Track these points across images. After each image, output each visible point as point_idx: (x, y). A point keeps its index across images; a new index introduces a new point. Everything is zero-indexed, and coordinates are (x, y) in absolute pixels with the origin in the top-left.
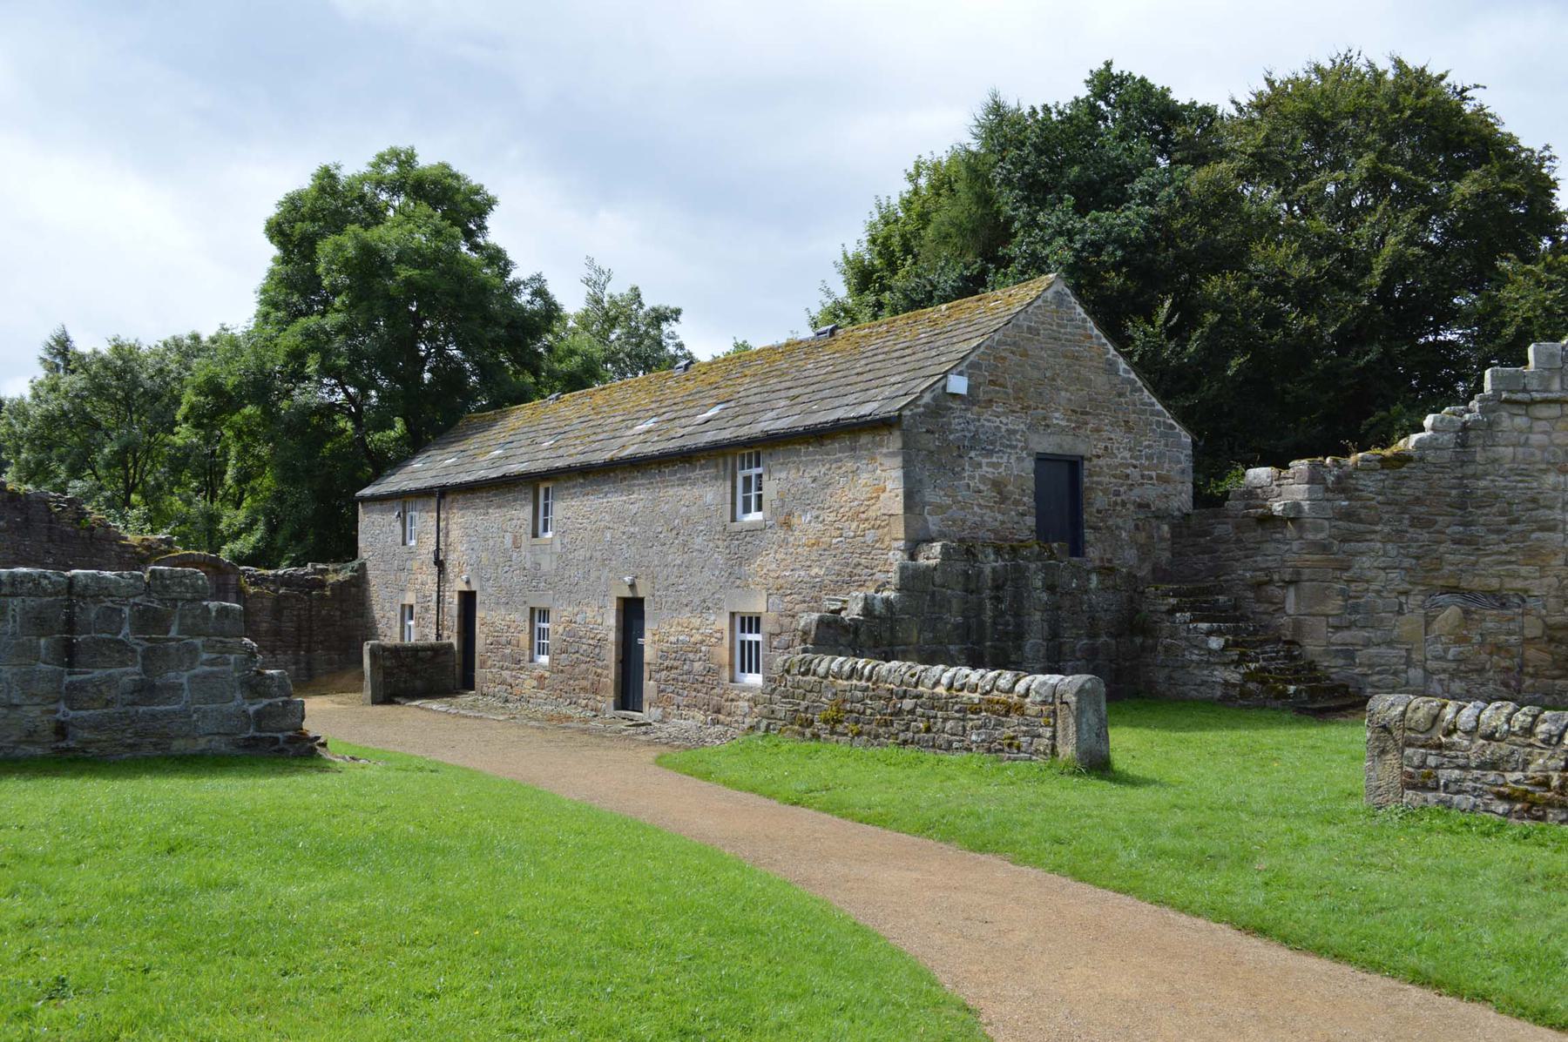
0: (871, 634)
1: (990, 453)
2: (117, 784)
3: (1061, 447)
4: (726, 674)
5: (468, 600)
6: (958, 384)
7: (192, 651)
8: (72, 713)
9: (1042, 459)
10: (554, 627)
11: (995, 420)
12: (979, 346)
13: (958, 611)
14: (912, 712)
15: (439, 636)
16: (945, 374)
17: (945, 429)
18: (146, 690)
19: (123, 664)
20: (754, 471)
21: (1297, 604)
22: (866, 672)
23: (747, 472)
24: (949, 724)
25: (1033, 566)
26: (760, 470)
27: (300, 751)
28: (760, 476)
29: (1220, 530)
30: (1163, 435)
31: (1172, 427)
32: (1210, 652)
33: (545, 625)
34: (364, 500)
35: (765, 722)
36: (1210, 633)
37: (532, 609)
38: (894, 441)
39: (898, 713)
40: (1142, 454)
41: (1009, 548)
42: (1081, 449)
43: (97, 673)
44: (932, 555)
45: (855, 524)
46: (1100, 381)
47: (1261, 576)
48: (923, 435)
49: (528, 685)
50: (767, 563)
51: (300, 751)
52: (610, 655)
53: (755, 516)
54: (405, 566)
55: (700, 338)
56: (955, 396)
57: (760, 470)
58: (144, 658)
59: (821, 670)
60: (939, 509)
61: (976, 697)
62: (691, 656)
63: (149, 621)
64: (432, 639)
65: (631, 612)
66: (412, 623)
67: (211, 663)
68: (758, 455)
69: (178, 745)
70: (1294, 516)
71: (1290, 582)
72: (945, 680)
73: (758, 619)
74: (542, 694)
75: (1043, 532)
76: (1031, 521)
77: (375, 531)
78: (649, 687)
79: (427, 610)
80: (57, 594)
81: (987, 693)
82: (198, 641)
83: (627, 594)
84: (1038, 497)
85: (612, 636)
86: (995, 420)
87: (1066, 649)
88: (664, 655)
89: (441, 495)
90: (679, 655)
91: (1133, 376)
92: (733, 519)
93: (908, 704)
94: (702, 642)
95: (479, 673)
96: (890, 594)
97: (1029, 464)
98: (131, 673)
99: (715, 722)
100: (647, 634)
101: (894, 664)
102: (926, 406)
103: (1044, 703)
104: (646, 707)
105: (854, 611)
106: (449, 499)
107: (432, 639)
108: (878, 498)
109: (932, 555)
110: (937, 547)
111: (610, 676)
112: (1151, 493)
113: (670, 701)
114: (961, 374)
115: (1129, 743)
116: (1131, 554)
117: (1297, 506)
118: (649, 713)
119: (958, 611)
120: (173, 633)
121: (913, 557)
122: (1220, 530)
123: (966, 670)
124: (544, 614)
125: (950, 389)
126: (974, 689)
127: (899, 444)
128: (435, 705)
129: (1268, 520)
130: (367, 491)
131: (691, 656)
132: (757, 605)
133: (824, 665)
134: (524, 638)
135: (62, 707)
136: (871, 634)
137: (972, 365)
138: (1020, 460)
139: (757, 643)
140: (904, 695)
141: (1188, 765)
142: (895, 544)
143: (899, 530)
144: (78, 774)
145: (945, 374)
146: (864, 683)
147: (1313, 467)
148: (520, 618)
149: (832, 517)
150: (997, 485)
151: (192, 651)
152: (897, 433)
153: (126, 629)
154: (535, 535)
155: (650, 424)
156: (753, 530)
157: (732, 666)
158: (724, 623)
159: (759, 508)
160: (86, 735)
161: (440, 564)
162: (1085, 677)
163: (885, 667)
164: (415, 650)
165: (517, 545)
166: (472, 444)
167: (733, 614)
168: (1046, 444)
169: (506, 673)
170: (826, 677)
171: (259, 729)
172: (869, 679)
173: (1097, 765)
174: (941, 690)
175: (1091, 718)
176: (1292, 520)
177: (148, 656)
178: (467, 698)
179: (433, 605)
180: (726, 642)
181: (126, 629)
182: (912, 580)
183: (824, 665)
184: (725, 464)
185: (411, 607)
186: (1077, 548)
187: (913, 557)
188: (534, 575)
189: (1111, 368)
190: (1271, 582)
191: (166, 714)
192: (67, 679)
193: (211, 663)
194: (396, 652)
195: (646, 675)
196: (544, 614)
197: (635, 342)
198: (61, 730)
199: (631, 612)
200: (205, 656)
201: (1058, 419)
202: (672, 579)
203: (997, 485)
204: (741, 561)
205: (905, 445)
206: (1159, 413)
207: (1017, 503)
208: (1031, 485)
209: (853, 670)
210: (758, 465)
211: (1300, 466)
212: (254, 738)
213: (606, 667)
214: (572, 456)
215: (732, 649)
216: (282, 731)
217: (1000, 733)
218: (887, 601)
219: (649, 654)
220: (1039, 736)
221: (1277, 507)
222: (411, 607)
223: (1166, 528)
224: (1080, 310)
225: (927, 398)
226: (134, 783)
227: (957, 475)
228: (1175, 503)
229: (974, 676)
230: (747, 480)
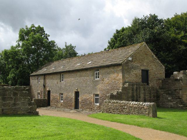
0: (119, 97)
1: (135, 69)
2: (176, 113)
3: (145, 68)
4: (93, 103)
5: (49, 92)
6: (130, 59)
7: (21, 98)
8: (4, 108)
9: (142, 70)
10: (64, 96)
11: (135, 64)
12: (133, 53)
13: (130, 93)
14: (126, 108)
15: (44, 98)
16: (128, 57)
17: (128, 66)
18: (15, 104)
19: (11, 100)
20: (98, 72)
21: (182, 93)
22: (119, 102)
23: (96, 72)
24: (132, 110)
25: (142, 87)
26: (98, 72)
27: (37, 114)
28: (98, 73)
29: (170, 81)
30: (161, 67)
31: (162, 65)
32: (168, 100)
33: (62, 96)
34: (31, 76)
35: (102, 110)
36: (169, 97)
37: (60, 93)
38: (121, 68)
39: (124, 108)
40: (157, 70)
41: (137, 84)
42: (148, 69)
43: (8, 102)
44: (127, 85)
45: (116, 80)
46: (151, 59)
47: (176, 88)
48: (124, 67)
49: (59, 105)
50: (100, 86)
51: (37, 114)
52: (73, 100)
53: (98, 79)
54: (37, 86)
55: (80, 52)
56: (130, 61)
57: (98, 72)
58: (14, 100)
59: (112, 102)
60: (127, 78)
61: (137, 106)
62: (87, 101)
63: (15, 94)
64: (43, 98)
65: (77, 94)
66: (39, 95)
67: (24, 100)
68: (98, 69)
69: (19, 113)
70: (181, 79)
71: (180, 90)
72: (131, 103)
73: (98, 95)
74: (62, 106)
75: (143, 81)
76: (141, 80)
77: (33, 82)
78: (80, 105)
79: (42, 93)
80: (2, 90)
81: (138, 105)
82: (22, 97)
83: (76, 91)
84: (142, 76)
85: (74, 98)
86: (135, 64)
87: (146, 99)
88: (82, 100)
89: (45, 75)
90: (86, 100)
91: (156, 58)
92: (94, 79)
93: (126, 107)
94: (89, 98)
95: (51, 103)
96: (120, 91)
97: (141, 71)
98: (12, 102)
99: (91, 111)
100: (80, 97)
101: (123, 101)
102: (125, 62)
103: (147, 107)
104: (79, 109)
105: (115, 93)
106: (46, 76)
107: (43, 98)
108: (118, 76)
109: (127, 85)
110: (128, 84)
111: (73, 104)
112: (159, 75)
113: (84, 108)
114: (130, 57)
115: (159, 114)
116: (156, 85)
117: (181, 78)
118: (80, 109)
119: (130, 93)
120: (18, 96)
121: (124, 85)
122: (170, 81)
123: (135, 102)
124: (62, 94)
125: (129, 60)
126: (136, 105)
127: (121, 68)
128: (44, 108)
129: (177, 80)
130: (34, 74)
131: (87, 101)
132: (98, 93)
133: (112, 101)
134: (59, 98)
135: (3, 107)
136: (119, 97)
137: (133, 56)
138: (139, 70)
139: (98, 98)
140: (125, 106)
141: (167, 117)
142: (121, 83)
143: (121, 81)
144: (15, 116)
145: (128, 57)
146: (119, 104)
147: (184, 72)
148: (58, 95)
149: (110, 79)
150: (136, 74)
151: (21, 98)
152: (121, 66)
153: (12, 95)
154: (60, 82)
155: (79, 64)
156: (97, 81)
157: (94, 102)
158: (92, 95)
159: (98, 77)
160: (6, 111)
161: (44, 86)
162: (154, 103)
163: (122, 102)
164: (40, 100)
165: (57, 83)
166: (49, 67)
167: (94, 94)
168: (143, 68)
169: (56, 103)
170: (112, 103)
171: (30, 110)
172: (119, 103)
173: (155, 116)
174: (131, 105)
175: (154, 109)
176: (181, 80)
177: (15, 99)
178: (49, 107)
179: (43, 92)
180: (93, 98)
181: (12, 95)
182: (124, 89)
183: (112, 101)
184: (93, 71)
185: (39, 93)
186: (148, 84)
187: (124, 85)
188: (61, 88)
189: (153, 56)
190: (177, 89)
191: (17, 108)
192: (3, 103)
193: (24, 100)
194: (38, 100)
195: (79, 104)
196: (62, 94)
197: (70, 53)
198: (3, 110)
199: (77, 94)
200: (23, 99)
201: (145, 64)
202: (84, 89)
203: (136, 74)
204: (95, 86)
205: (122, 68)
206: (160, 63)
207: (139, 77)
208: (141, 74)
209: (117, 102)
210: (98, 71)
211: (182, 72)
212: (30, 112)
213: (73, 102)
214: (67, 69)
215: (94, 99)
216: (34, 110)
217: (139, 111)
218: (120, 92)
219: (80, 100)
220: (146, 112)
221: (178, 78)
222: (39, 93)
223: (161, 81)
224: (148, 47)
225: (126, 61)
226: (30, 117)
227: (130, 73)
228: (162, 77)
229: (136, 103)
230: (96, 73)
